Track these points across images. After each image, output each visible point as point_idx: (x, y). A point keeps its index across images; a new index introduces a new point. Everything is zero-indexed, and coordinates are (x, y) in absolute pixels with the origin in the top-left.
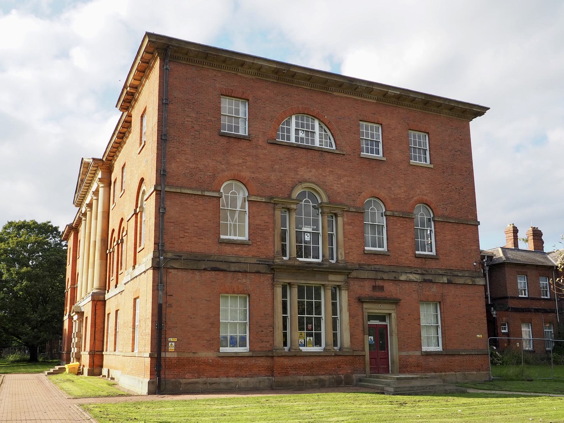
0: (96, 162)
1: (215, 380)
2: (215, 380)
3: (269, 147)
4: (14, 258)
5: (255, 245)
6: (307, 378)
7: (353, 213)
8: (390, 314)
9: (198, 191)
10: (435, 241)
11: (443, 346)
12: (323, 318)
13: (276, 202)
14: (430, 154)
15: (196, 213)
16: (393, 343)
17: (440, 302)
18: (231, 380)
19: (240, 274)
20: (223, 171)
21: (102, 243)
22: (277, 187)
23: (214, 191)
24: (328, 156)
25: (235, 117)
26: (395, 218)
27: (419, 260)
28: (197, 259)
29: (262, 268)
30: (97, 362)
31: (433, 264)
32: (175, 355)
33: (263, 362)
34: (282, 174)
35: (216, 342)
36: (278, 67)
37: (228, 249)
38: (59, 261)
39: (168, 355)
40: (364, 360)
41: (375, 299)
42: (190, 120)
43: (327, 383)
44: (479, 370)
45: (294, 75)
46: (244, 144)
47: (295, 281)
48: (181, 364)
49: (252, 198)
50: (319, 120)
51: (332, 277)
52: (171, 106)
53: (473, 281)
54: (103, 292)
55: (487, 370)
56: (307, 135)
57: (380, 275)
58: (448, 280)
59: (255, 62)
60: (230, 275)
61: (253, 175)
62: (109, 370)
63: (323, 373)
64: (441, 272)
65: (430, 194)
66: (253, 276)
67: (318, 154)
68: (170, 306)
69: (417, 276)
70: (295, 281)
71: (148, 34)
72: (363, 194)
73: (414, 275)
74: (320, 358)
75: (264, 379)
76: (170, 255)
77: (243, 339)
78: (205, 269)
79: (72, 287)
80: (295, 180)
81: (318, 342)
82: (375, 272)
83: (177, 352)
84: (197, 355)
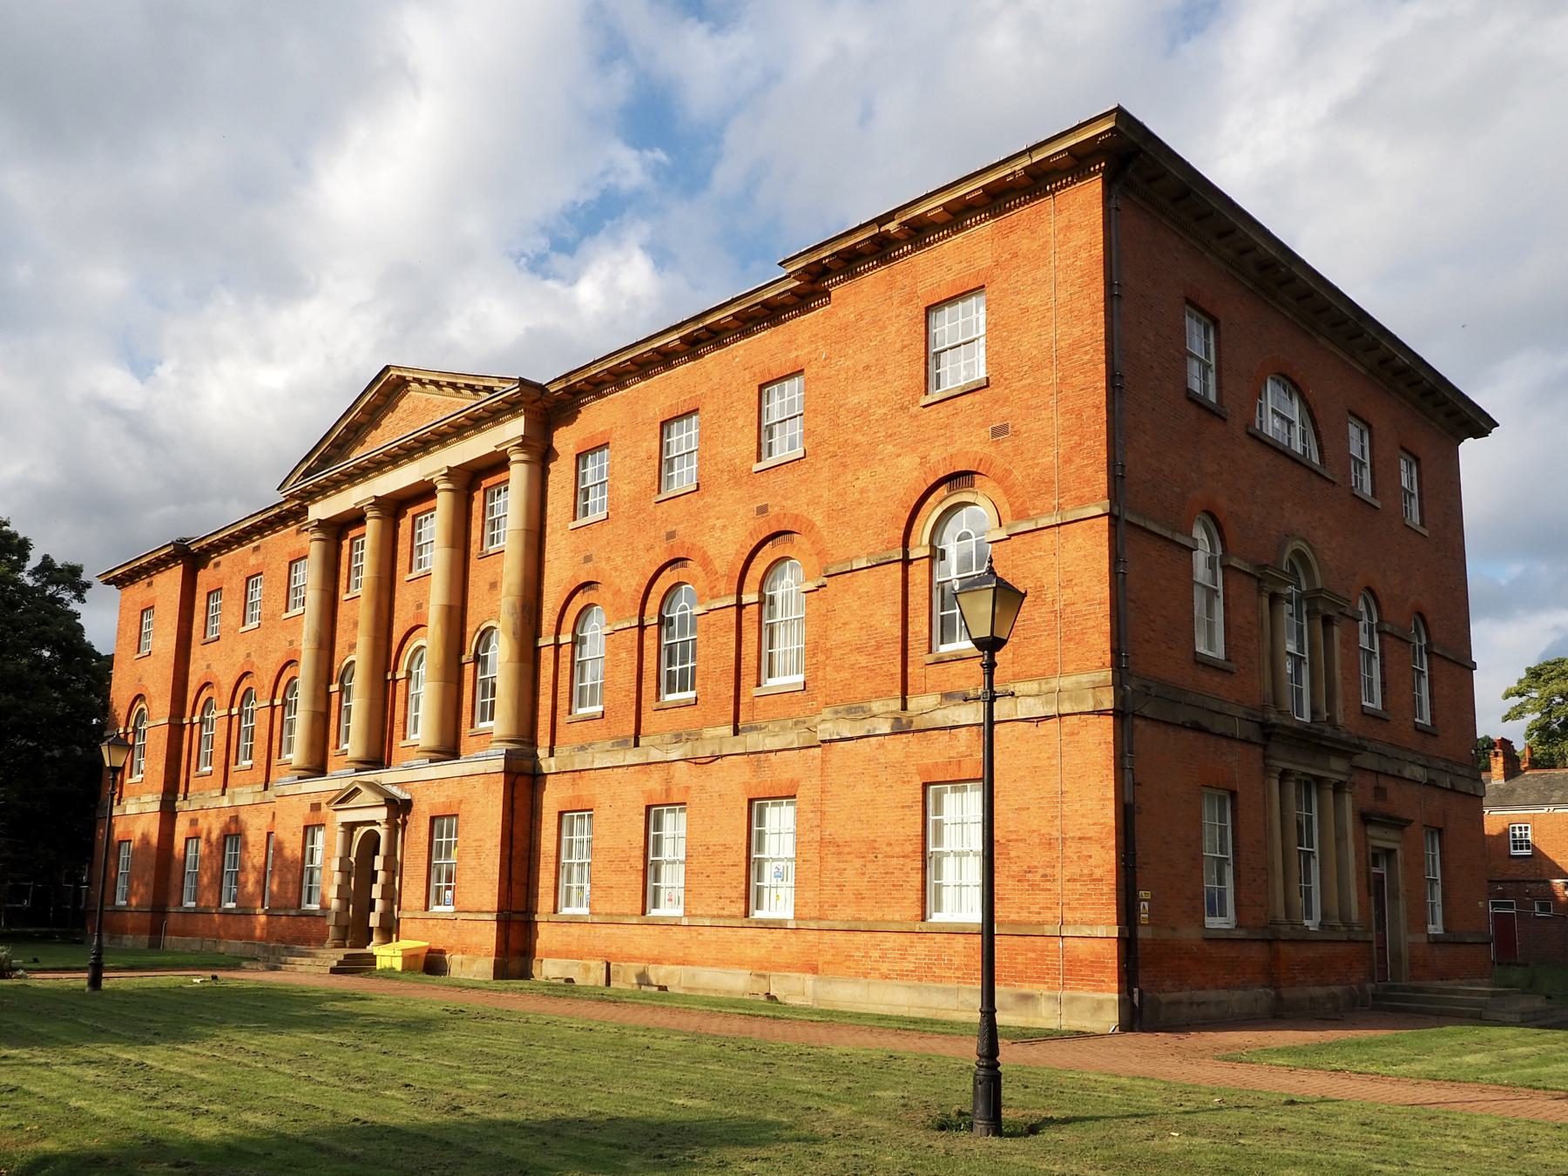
2: (1200, 995)
8: (1390, 853)
11: (1237, 912)
33: (1257, 953)
62: (608, 965)
71: (1120, 113)
75: (1259, 995)
78: (1183, 726)
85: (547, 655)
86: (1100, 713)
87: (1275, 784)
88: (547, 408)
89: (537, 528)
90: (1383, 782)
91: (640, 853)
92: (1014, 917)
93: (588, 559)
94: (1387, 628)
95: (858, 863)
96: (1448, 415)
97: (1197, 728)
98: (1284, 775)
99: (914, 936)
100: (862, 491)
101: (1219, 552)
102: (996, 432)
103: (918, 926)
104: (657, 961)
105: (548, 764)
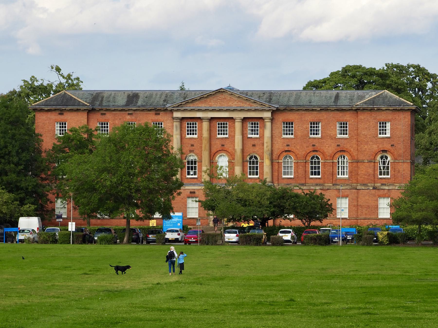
95: (366, 209)
100: (366, 149)
102: (392, 145)
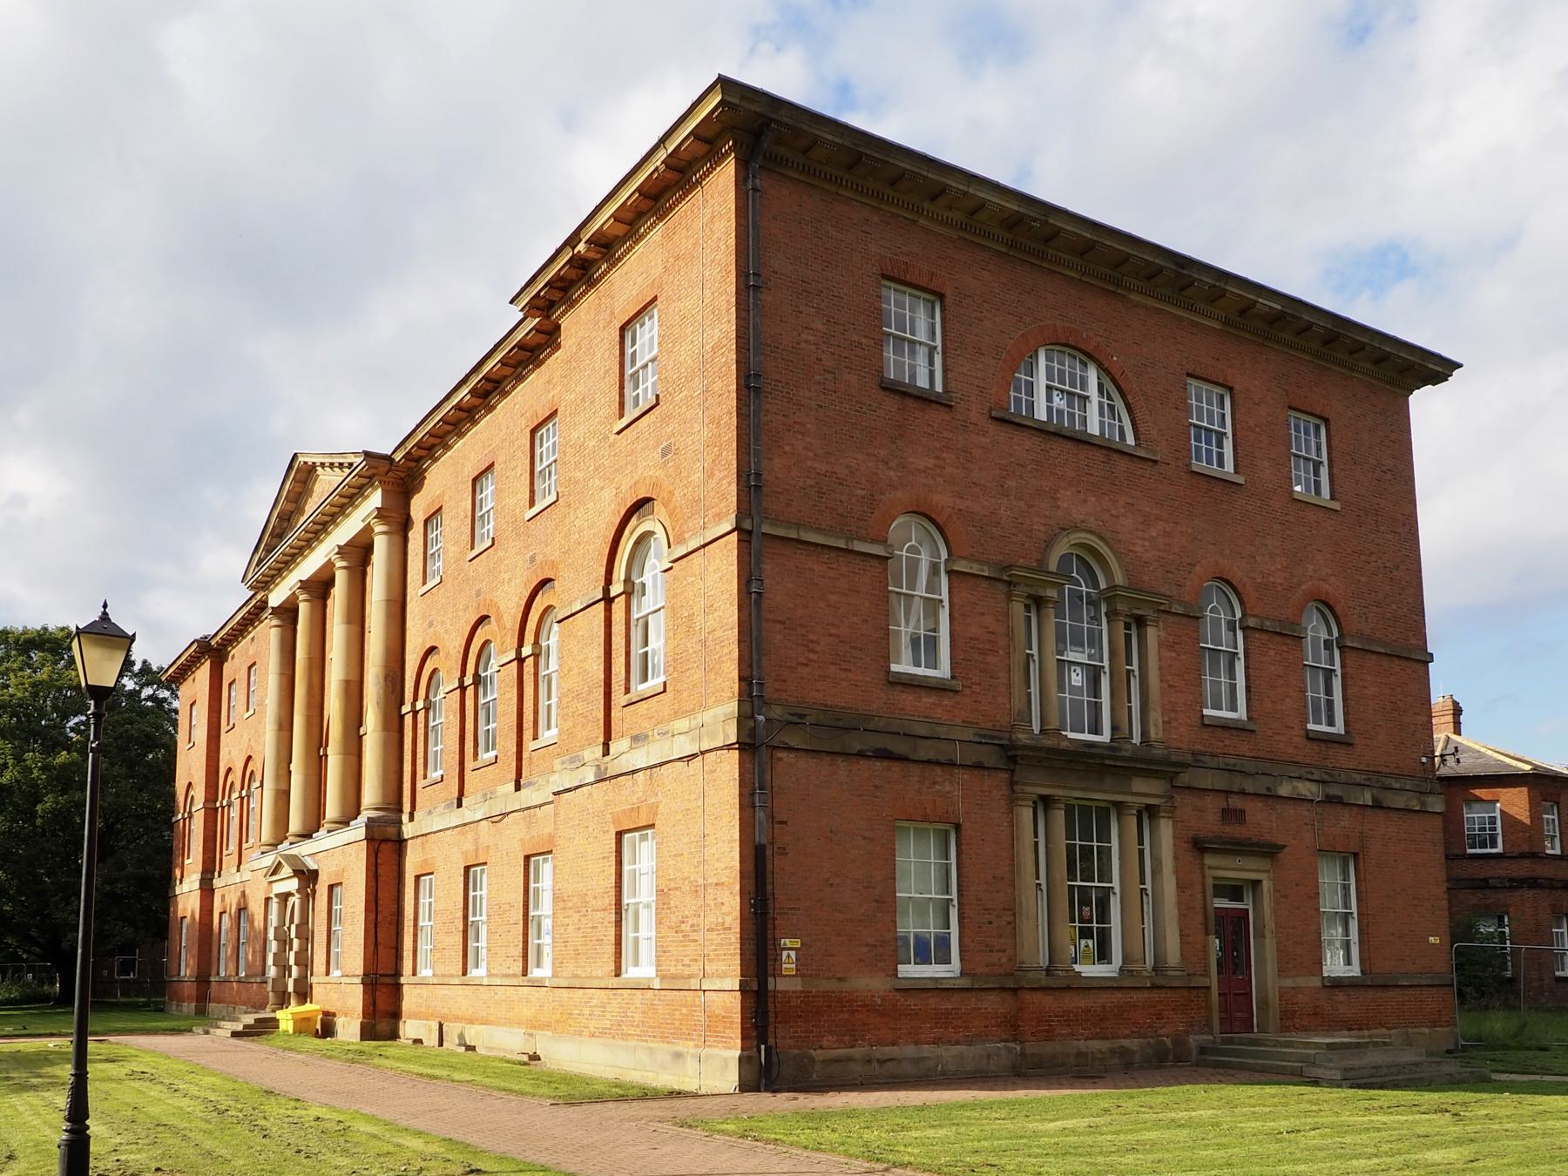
0: (374, 462)
1: (889, 1051)
2: (889, 1051)
3: (993, 428)
4: (31, 725)
5: (968, 691)
6: (1096, 1045)
7: (1176, 619)
8: (1256, 884)
9: (838, 538)
10: (1345, 699)
12: (1117, 890)
13: (1015, 580)
14: (1331, 475)
15: (833, 598)
16: (1264, 959)
17: (1356, 855)
18: (926, 1050)
19: (938, 770)
20: (892, 486)
21: (387, 686)
22: (1014, 539)
23: (873, 541)
24: (1123, 464)
25: (895, 337)
26: (1265, 637)
27: (1315, 746)
28: (840, 724)
29: (989, 757)
30: (382, 1003)
31: (1341, 758)
32: (796, 985)
33: (993, 1003)
34: (1022, 504)
35: (890, 951)
36: (1023, 211)
37: (907, 699)
38: (148, 736)
39: (782, 985)
40: (1207, 999)
41: (1232, 844)
42: (812, 338)
43: (1137, 1058)
44: (1434, 1024)
45: (1052, 236)
46: (936, 416)
47: (1060, 792)
48: (812, 1008)
49: (960, 566)
50: (1101, 367)
51: (1139, 785)
52: (767, 297)
53: (1423, 803)
54: (393, 816)
55: (1451, 1023)
56: (1070, 405)
57: (1238, 783)
58: (1374, 799)
59: (971, 190)
60: (916, 770)
61: (960, 504)
62: (441, 1026)
63: (1127, 1032)
64: (1358, 778)
65: (1333, 579)
66: (965, 775)
67: (1099, 456)
68: (783, 851)
69: (1313, 787)
70: (1060, 792)
71: (723, 82)
72: (1198, 568)
73: (1308, 784)
74: (1119, 995)
75: (999, 1049)
76: (777, 712)
77: (944, 942)
79: (209, 805)
80: (1052, 522)
81: (1103, 955)
82: (1227, 774)
83: (803, 976)
84: (846, 986)
85: (408, 720)
86: (729, 747)
87: (1026, 814)
88: (399, 475)
89: (400, 599)
90: (1236, 802)
91: (460, 914)
92: (673, 970)
93: (431, 625)
94: (1252, 622)
95: (576, 917)
96: (1377, 362)
97: (883, 755)
98: (1047, 802)
99: (610, 992)
101: (944, 555)
103: (614, 982)
104: (471, 1022)
105: (408, 830)
